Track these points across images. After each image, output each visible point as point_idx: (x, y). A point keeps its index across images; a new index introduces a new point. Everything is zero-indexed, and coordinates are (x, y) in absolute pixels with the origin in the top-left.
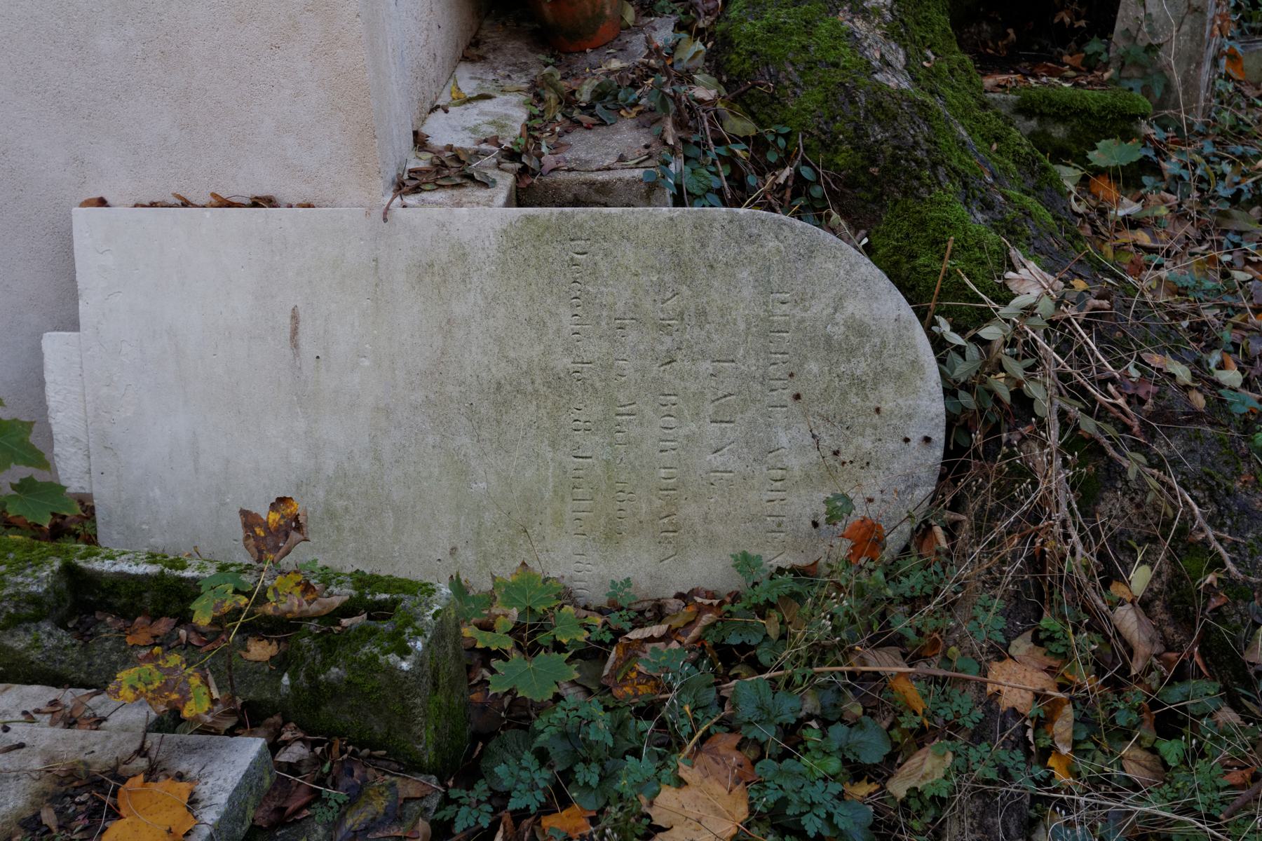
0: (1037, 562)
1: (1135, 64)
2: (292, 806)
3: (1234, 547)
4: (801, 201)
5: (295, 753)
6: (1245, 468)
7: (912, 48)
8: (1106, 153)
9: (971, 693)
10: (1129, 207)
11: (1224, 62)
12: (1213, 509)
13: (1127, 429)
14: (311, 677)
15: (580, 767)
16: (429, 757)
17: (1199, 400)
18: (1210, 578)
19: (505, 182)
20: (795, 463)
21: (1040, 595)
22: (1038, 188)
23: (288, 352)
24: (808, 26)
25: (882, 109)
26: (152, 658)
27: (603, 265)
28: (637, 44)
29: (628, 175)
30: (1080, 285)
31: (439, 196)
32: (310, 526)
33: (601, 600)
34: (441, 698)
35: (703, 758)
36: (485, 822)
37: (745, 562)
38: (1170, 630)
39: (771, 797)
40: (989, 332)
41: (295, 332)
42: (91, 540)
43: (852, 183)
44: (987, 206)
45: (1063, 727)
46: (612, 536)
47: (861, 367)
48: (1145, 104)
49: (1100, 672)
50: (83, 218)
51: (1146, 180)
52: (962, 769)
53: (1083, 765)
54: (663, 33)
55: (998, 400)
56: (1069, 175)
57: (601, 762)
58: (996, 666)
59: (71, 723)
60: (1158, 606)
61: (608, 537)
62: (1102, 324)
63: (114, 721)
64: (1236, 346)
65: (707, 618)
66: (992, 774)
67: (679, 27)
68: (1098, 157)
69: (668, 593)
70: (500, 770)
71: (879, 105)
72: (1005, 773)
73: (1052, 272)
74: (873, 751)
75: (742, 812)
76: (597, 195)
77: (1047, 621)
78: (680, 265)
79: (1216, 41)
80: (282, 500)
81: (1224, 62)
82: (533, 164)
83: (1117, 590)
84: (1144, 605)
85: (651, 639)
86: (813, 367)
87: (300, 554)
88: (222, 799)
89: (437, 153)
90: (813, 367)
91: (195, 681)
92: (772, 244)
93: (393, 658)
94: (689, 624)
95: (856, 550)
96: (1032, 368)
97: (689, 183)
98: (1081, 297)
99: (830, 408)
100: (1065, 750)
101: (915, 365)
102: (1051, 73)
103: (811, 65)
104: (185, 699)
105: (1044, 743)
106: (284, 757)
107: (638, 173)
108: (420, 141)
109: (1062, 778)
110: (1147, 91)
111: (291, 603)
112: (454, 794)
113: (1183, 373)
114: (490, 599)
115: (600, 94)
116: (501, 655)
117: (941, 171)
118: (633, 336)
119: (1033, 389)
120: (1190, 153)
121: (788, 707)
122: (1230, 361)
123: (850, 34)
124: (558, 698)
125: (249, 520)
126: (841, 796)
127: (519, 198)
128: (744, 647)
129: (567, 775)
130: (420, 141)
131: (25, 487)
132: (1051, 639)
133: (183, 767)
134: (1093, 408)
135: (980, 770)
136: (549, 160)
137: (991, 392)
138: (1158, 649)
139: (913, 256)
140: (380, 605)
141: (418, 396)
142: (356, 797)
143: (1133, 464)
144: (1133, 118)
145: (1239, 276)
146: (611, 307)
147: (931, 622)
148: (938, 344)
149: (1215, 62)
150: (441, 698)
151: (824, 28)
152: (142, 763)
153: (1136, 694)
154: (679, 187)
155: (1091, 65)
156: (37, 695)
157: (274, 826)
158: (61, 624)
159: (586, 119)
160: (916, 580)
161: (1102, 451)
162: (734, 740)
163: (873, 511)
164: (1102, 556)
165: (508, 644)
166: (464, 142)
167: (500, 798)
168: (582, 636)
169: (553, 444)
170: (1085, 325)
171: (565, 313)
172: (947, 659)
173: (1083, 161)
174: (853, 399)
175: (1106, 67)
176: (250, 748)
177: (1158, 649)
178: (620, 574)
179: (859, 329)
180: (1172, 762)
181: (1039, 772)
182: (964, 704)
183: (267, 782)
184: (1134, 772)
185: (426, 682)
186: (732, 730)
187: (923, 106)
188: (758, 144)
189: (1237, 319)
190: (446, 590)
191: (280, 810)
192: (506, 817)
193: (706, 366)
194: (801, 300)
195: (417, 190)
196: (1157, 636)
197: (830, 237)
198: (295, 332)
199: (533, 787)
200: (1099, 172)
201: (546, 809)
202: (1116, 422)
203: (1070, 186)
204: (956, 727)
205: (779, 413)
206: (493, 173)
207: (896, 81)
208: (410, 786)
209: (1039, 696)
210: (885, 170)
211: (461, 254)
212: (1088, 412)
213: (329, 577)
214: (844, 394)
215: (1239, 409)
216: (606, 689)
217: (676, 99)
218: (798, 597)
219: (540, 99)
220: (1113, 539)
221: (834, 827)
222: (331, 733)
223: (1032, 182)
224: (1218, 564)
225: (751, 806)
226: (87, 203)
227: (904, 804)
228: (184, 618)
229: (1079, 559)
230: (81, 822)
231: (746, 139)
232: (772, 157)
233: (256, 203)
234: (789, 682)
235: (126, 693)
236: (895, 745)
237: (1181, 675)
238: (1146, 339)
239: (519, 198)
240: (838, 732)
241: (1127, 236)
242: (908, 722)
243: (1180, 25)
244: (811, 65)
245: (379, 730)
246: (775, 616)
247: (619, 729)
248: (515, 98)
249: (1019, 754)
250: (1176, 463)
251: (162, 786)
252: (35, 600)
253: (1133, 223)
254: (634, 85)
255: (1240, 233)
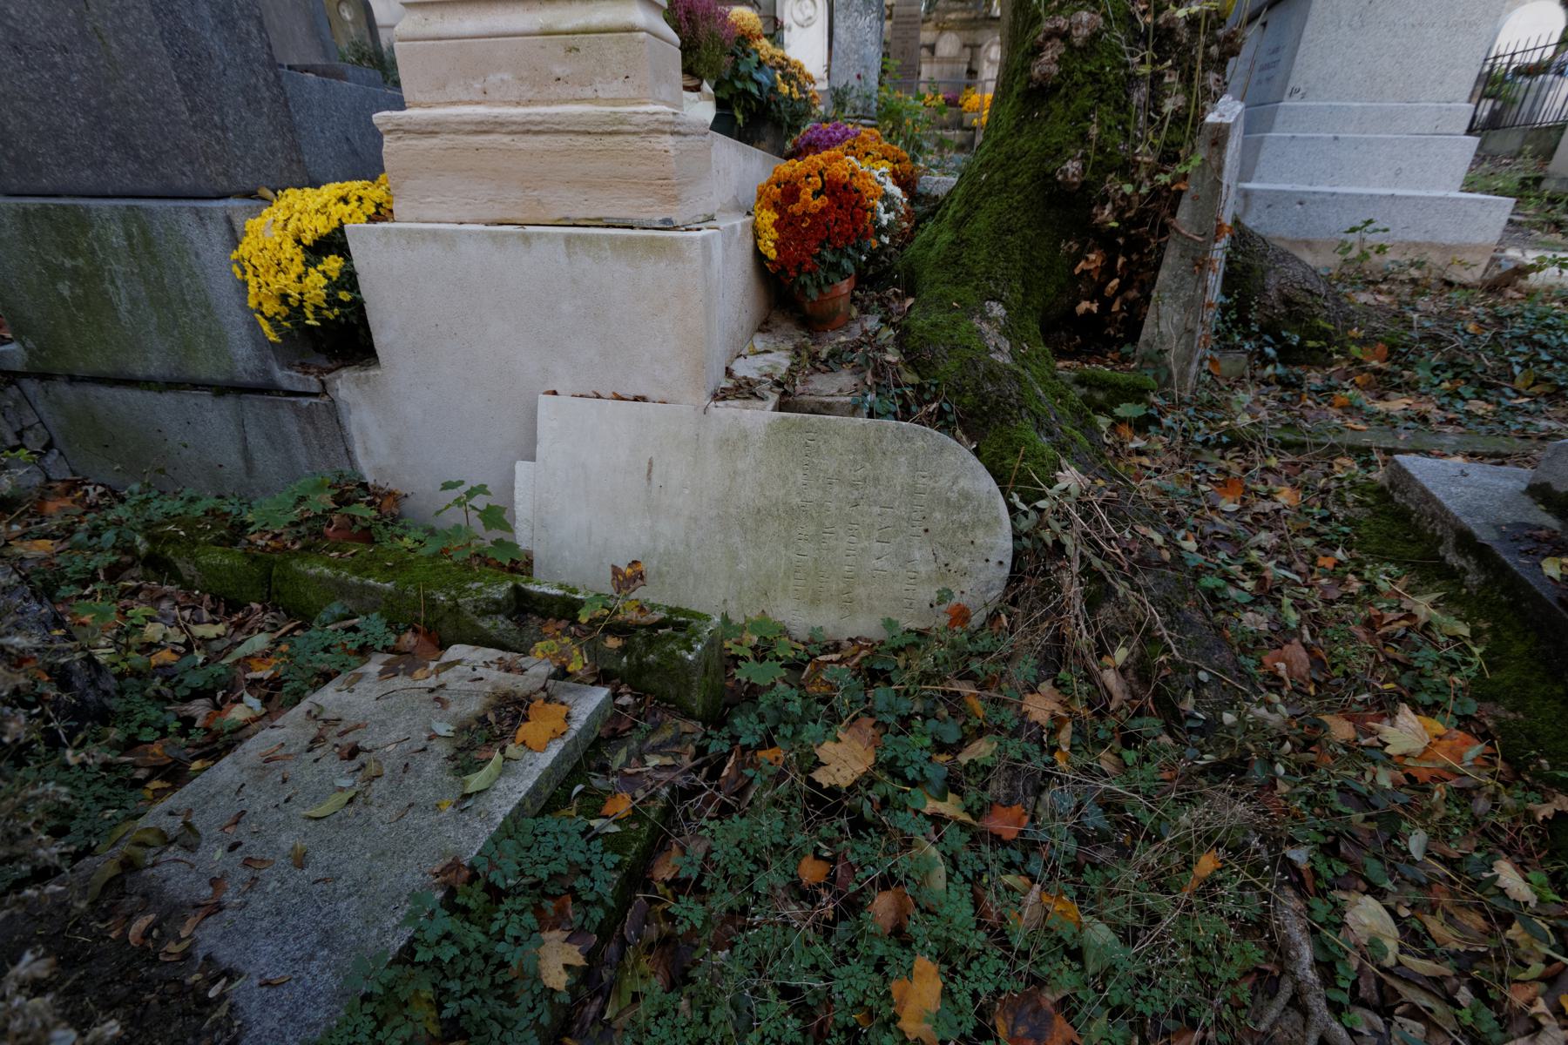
0: (1059, 638)
1: (1150, 360)
2: (621, 728)
3: (1179, 642)
4: (941, 423)
5: (626, 700)
6: (1191, 597)
7: (1014, 342)
8: (1126, 410)
9: (1013, 711)
10: (1138, 443)
11: (1207, 363)
12: (1168, 618)
13: (1121, 567)
14: (639, 658)
15: (782, 726)
16: (698, 711)
17: (1166, 555)
18: (1163, 658)
19: (774, 398)
20: (923, 569)
21: (1060, 659)
22: (1083, 427)
23: (645, 481)
24: (955, 325)
25: (992, 374)
26: (555, 637)
27: (823, 448)
28: (856, 330)
29: (843, 399)
30: (1101, 483)
31: (736, 403)
32: (648, 579)
33: (806, 638)
34: (709, 679)
35: (854, 730)
36: (726, 750)
37: (889, 624)
38: (1136, 687)
39: (889, 754)
40: (1041, 504)
41: (650, 471)
42: (530, 574)
43: (971, 414)
44: (1050, 433)
45: (1065, 736)
46: (815, 601)
47: (966, 518)
48: (1153, 383)
49: (1090, 706)
50: (544, 400)
51: (1152, 428)
52: (1002, 751)
53: (1074, 758)
54: (872, 323)
55: (1045, 545)
56: (1103, 422)
57: (794, 724)
58: (1029, 696)
59: (508, 670)
60: (1130, 672)
61: (812, 602)
62: (1112, 506)
63: (531, 671)
64: (1196, 528)
65: (864, 653)
66: (1019, 757)
67: (881, 320)
68: (1119, 412)
69: (843, 637)
70: (737, 721)
71: (991, 372)
72: (1027, 757)
73: (1085, 474)
74: (951, 734)
75: (871, 760)
76: (826, 409)
77: (1063, 674)
78: (867, 452)
79: (1201, 350)
80: (635, 562)
81: (1207, 363)
82: (790, 389)
83: (1106, 660)
84: (1122, 671)
85: (831, 662)
86: (938, 515)
87: (641, 593)
88: (584, 718)
89: (738, 380)
90: (938, 515)
91: (576, 652)
92: (920, 443)
93: (684, 652)
94: (854, 656)
95: (953, 622)
96: (1065, 528)
97: (877, 407)
98: (1100, 489)
99: (945, 539)
100: (1065, 749)
101: (997, 519)
102: (1098, 362)
103: (954, 346)
104: (569, 661)
105: (1054, 743)
106: (619, 701)
107: (849, 399)
108: (729, 373)
109: (1062, 764)
110: (1156, 377)
111: (632, 615)
112: (710, 732)
113: (1158, 539)
114: (743, 628)
115: (832, 355)
116: (745, 659)
117: (1024, 411)
118: (836, 489)
119: (1067, 540)
120: (1179, 414)
121: (904, 706)
122: (1191, 536)
123: (979, 331)
124: (774, 684)
125: (616, 571)
126: (930, 759)
127: (781, 407)
128: (883, 671)
129: (775, 729)
130: (729, 373)
131: (498, 543)
132: (1064, 685)
133: (565, 699)
134: (1100, 553)
135: (1011, 753)
136: (799, 388)
137: (1041, 539)
138: (1127, 696)
139: (1003, 458)
140: (681, 624)
141: (713, 513)
142: (656, 728)
143: (1122, 588)
144: (1146, 391)
145: (1202, 488)
146: (826, 472)
147: (993, 668)
148: (1012, 509)
149: (1201, 363)
150: (709, 679)
151: (963, 327)
152: (544, 694)
153: (1112, 722)
154: (871, 409)
155: (1125, 359)
156: (493, 654)
157: (610, 738)
158: (509, 617)
159: (823, 367)
160: (987, 642)
161: (1104, 579)
162: (872, 721)
163: (964, 601)
164: (1098, 639)
165: (749, 654)
166: (753, 375)
167: (734, 738)
168: (791, 654)
169: (786, 547)
170: (1102, 506)
171: (799, 472)
172: (1000, 690)
173: (1111, 414)
174: (959, 535)
175: (1133, 360)
176: (603, 693)
177: (1127, 696)
178: (817, 623)
179: (967, 496)
180: (1129, 763)
181: (1047, 758)
182: (1008, 716)
183: (609, 714)
184: (1106, 766)
185: (701, 669)
186: (871, 716)
187: (1017, 374)
188: (920, 389)
189: (1198, 512)
190: (717, 619)
191: (615, 730)
192: (737, 748)
193: (876, 510)
194: (933, 477)
195: (724, 399)
196: (1127, 689)
197: (954, 442)
198: (650, 471)
199: (754, 733)
200: (1121, 421)
201: (760, 747)
202: (1114, 562)
203: (1104, 428)
204: (1001, 728)
205: (916, 540)
206: (767, 393)
207: (1002, 359)
208: (687, 726)
209: (1054, 717)
210: (991, 408)
211: (745, 436)
212: (1099, 556)
213: (653, 607)
214: (954, 532)
215: (1191, 563)
216: (801, 687)
217: (875, 360)
218: (917, 646)
219: (798, 354)
220: (1106, 630)
221: (923, 776)
222: (646, 692)
223: (1079, 423)
224: (1168, 650)
225: (877, 759)
226: (547, 393)
227: (966, 768)
228: (574, 621)
229: (1084, 640)
230: (508, 721)
231: (913, 386)
232: (927, 397)
233: (636, 399)
234: (907, 692)
235: (539, 654)
236: (965, 735)
237: (1140, 713)
238: (1138, 518)
239: (781, 407)
240: (932, 723)
241: (1135, 460)
242: (974, 722)
243: (1179, 339)
244: (954, 346)
245: (673, 692)
246: (903, 656)
247: (806, 708)
248: (784, 354)
249: (1036, 747)
250: (1148, 590)
251: (551, 707)
252: (496, 602)
253: (1139, 452)
254: (852, 351)
255: (1206, 463)
